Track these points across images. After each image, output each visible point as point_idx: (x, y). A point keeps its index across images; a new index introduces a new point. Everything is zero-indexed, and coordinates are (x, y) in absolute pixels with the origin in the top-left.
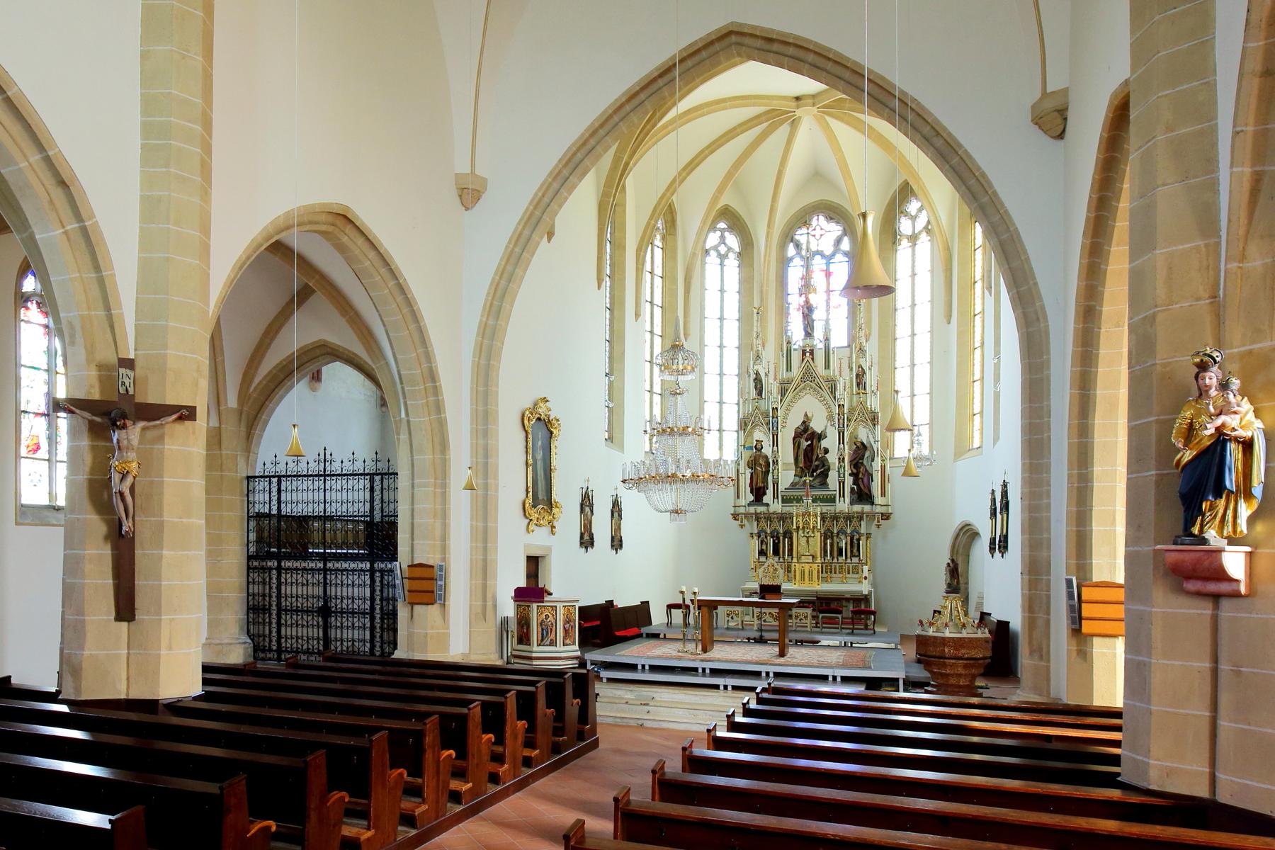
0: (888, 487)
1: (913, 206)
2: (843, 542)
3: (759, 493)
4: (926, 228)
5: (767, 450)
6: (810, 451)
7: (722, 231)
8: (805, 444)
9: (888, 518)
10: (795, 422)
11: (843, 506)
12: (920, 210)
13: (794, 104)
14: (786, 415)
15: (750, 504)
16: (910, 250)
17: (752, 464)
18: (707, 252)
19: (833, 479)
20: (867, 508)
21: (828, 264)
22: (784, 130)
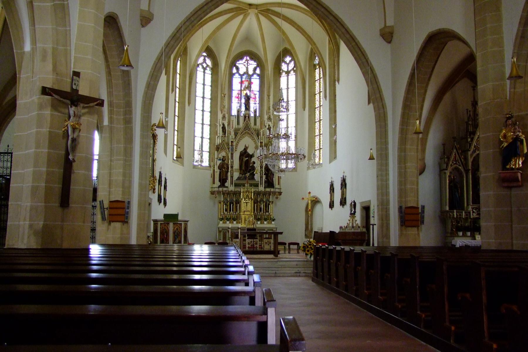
1: (288, 59)
2: (262, 205)
3: (223, 181)
4: (293, 69)
6: (247, 162)
7: (205, 57)
10: (241, 148)
11: (261, 188)
12: (290, 61)
13: (248, 7)
14: (237, 145)
15: (219, 187)
16: (286, 77)
17: (221, 167)
18: (198, 65)
19: (257, 177)
20: (272, 190)
22: (241, 17)
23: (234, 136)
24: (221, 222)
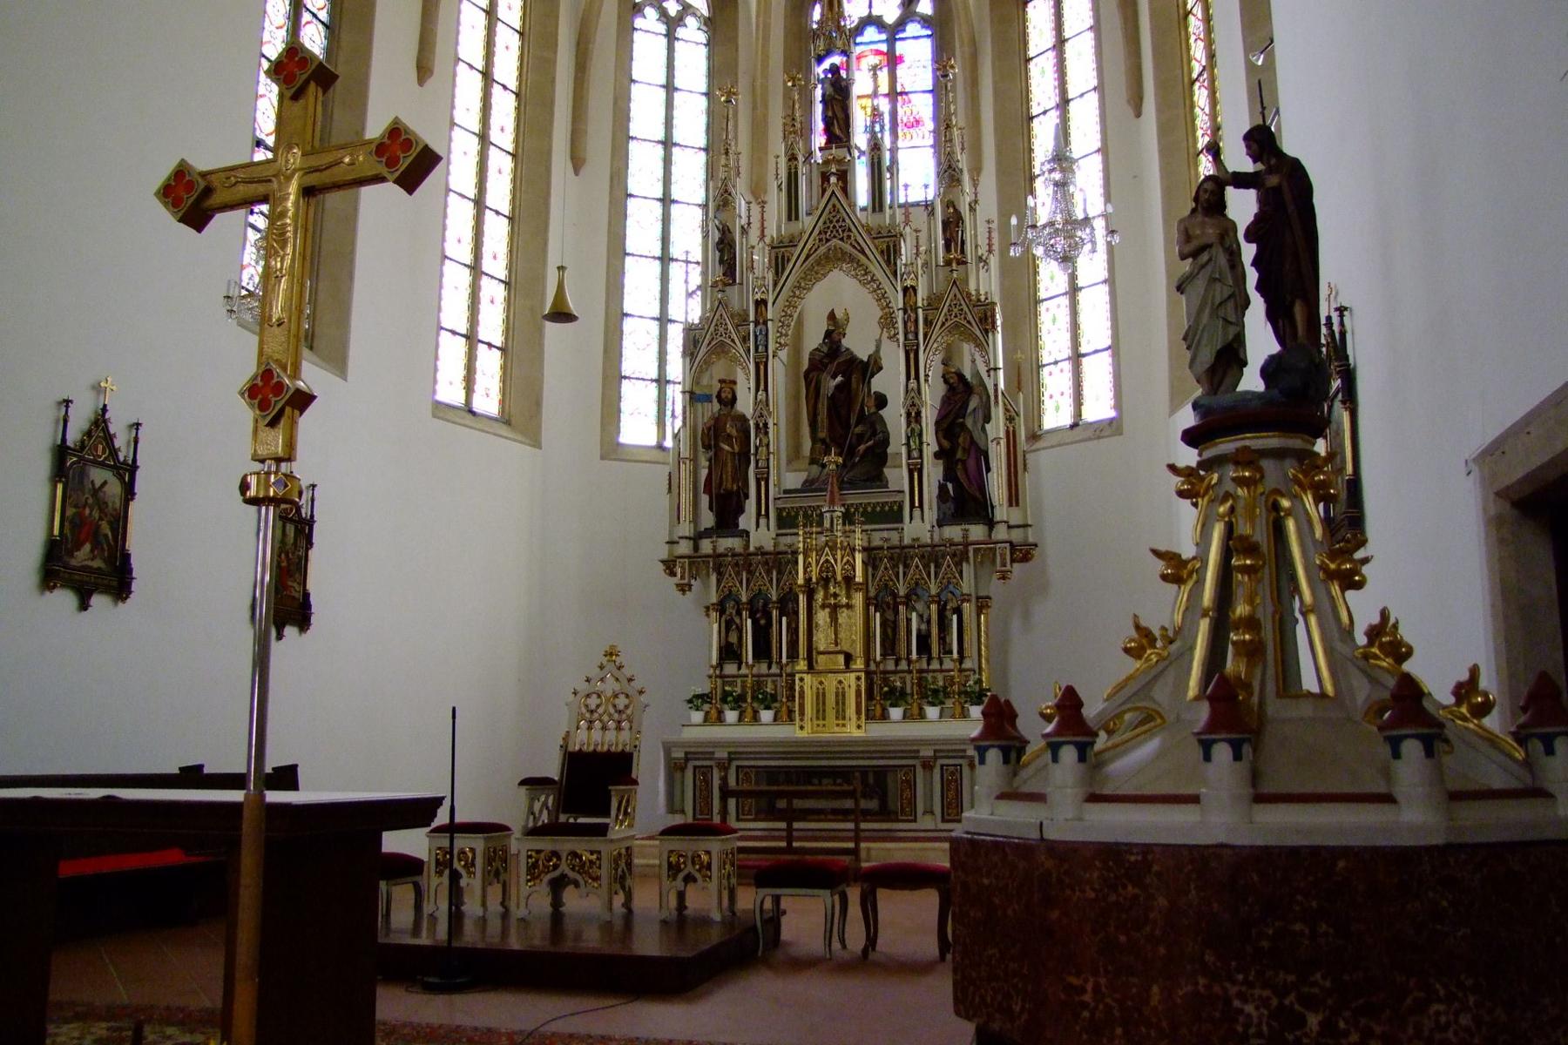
0: (1027, 481)
3: (727, 510)
5: (746, 404)
8: (831, 384)
9: (1026, 558)
11: (919, 528)
19: (897, 476)
20: (977, 532)
21: (891, 41)
23: (770, 276)
24: (697, 717)
